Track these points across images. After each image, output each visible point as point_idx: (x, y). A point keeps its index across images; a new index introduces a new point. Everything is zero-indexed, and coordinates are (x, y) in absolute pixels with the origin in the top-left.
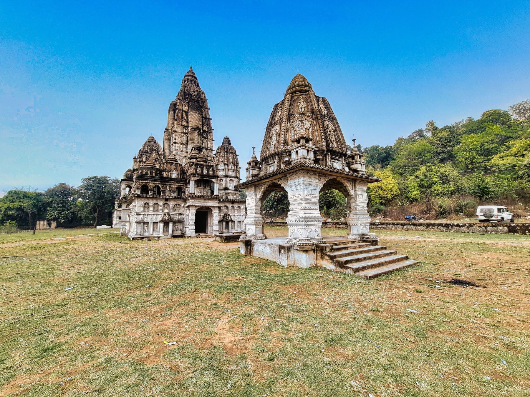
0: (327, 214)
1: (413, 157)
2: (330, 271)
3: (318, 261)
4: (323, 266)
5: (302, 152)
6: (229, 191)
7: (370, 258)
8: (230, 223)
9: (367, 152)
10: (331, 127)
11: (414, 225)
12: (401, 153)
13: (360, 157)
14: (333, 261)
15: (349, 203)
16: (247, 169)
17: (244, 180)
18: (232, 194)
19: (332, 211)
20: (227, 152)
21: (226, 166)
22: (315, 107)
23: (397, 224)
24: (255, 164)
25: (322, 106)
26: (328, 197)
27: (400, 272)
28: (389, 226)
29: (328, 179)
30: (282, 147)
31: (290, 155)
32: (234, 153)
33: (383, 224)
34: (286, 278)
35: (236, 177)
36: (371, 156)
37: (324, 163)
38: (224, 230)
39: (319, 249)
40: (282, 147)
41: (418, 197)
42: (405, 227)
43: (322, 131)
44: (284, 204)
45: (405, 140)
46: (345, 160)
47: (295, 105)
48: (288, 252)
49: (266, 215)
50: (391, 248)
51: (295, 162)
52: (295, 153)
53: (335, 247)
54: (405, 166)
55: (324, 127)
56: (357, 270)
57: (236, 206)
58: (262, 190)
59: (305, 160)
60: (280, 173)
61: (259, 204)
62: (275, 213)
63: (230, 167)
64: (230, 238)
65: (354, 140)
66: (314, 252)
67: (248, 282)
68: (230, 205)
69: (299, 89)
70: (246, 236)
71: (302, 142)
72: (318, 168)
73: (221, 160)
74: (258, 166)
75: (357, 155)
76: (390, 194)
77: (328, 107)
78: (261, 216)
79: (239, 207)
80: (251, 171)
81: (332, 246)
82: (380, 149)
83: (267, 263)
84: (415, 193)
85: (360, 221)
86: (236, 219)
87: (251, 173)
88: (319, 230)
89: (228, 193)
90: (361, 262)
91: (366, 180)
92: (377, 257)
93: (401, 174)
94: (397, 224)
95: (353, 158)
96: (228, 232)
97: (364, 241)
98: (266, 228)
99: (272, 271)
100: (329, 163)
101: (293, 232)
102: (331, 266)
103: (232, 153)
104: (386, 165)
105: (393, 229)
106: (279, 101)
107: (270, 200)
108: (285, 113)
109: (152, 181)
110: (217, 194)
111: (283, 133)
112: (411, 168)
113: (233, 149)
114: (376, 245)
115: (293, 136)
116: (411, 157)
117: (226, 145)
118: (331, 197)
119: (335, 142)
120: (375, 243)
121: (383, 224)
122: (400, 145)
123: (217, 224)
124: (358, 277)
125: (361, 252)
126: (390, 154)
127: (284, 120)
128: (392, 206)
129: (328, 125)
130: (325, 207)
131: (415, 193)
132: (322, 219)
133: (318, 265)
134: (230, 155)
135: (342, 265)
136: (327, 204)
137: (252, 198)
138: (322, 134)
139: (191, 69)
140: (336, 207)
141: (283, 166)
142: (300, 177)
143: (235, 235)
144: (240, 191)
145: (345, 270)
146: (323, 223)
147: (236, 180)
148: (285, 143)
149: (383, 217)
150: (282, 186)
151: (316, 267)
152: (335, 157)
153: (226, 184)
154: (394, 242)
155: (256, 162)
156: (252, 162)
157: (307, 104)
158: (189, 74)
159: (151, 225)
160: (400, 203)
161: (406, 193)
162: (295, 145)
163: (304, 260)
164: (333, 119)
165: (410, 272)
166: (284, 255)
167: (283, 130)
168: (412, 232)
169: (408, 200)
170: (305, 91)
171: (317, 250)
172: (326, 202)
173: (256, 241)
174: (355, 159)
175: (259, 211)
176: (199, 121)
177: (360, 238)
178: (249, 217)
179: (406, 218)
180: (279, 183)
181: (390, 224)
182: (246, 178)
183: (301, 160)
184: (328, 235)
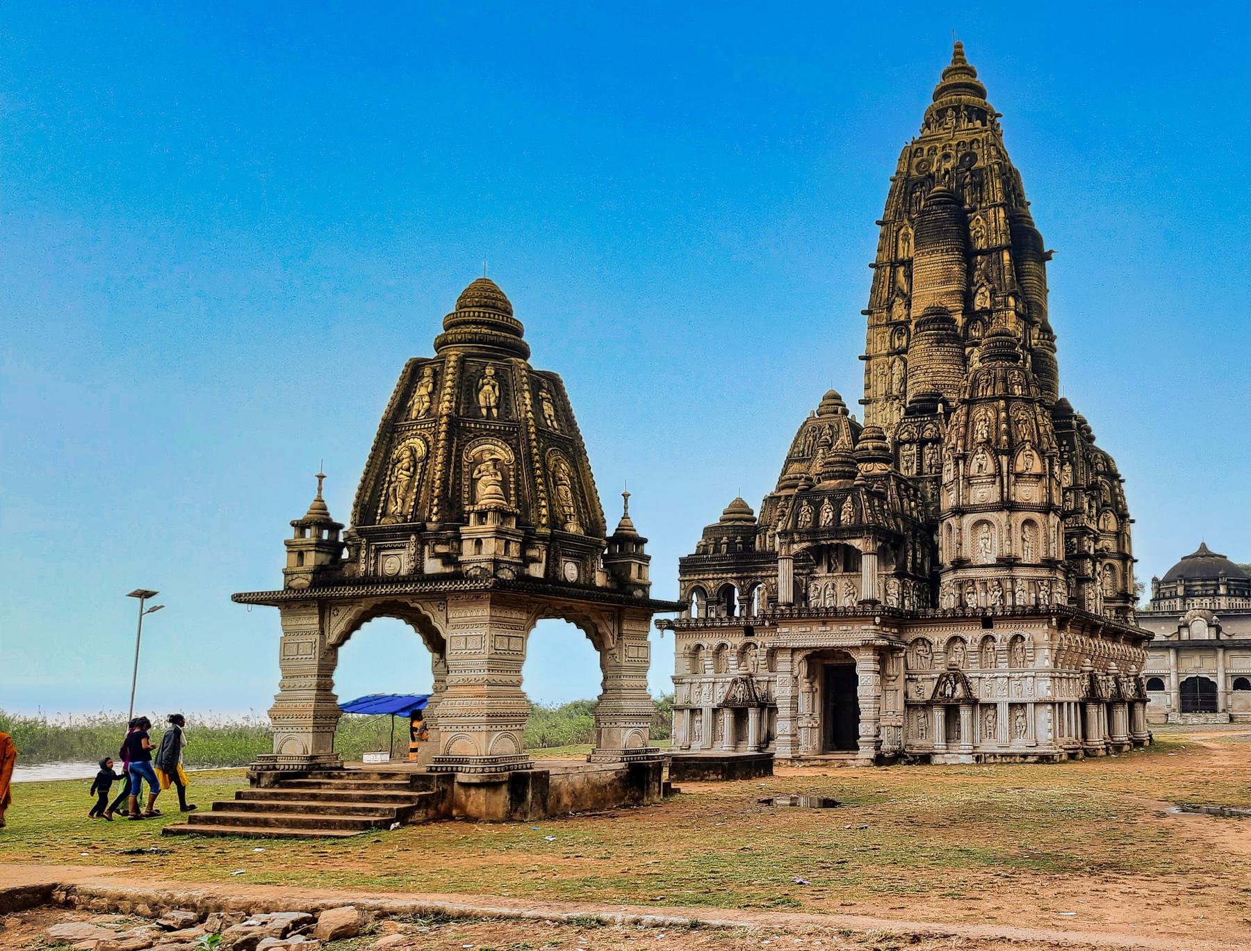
6: (971, 573)
8: (965, 713)
21: (1004, 460)
57: (1003, 633)
63: (974, 469)
64: (687, 767)
68: (973, 634)
69: (487, 334)
109: (716, 571)
139: (959, 52)
158: (951, 81)
159: (707, 715)
176: (947, 281)
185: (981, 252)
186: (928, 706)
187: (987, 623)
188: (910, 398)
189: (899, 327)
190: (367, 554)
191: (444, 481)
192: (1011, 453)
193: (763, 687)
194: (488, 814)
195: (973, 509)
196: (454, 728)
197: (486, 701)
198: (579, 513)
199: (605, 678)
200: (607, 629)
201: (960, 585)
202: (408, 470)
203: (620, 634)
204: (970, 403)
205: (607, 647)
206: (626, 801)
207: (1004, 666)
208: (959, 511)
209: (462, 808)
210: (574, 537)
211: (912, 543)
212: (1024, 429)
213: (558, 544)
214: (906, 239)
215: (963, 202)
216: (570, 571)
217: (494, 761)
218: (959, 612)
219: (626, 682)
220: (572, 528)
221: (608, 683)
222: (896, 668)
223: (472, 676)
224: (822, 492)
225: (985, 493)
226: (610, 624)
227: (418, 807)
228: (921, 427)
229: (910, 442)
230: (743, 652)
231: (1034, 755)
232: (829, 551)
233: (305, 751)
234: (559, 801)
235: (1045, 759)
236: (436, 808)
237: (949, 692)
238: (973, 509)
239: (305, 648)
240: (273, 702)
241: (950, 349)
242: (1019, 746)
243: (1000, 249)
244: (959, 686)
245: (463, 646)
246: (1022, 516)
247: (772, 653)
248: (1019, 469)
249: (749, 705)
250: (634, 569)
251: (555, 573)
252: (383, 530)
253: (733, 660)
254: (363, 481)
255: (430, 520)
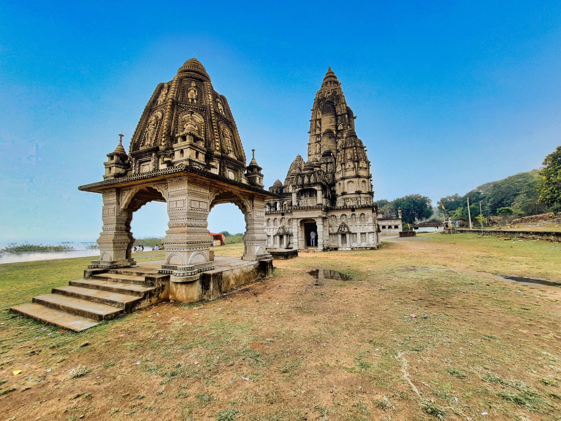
6: (347, 196)
8: (348, 236)
21: (356, 164)
57: (358, 213)
63: (347, 167)
68: (349, 213)
69: (195, 75)
139: (330, 69)
141: (162, 167)
152: (144, 159)
159: (272, 237)
176: (331, 122)
180: (155, 188)
185: (339, 115)
186: (336, 234)
187: (353, 210)
188: (322, 153)
189: (318, 136)
190: (135, 165)
191: (169, 127)
192: (358, 162)
193: (287, 229)
194: (187, 299)
195: (347, 178)
196: (171, 250)
197: (186, 235)
198: (234, 151)
199: (247, 225)
200: (247, 203)
201: (344, 199)
202: (154, 125)
203: (253, 206)
204: (345, 149)
205: (248, 211)
206: (259, 277)
207: (359, 222)
208: (343, 179)
209: (174, 294)
210: (231, 159)
211: (329, 188)
212: (361, 155)
213: (224, 160)
214: (319, 114)
215: (333, 103)
216: (231, 175)
217: (192, 268)
218: (345, 207)
219: (256, 226)
220: (231, 155)
221: (249, 227)
222: (326, 224)
223: (180, 222)
224: (304, 174)
225: (351, 173)
226: (249, 201)
227: (144, 298)
228: (327, 159)
229: (324, 163)
230: (281, 220)
232: (306, 191)
233: (111, 259)
234: (228, 283)
235: (372, 249)
236: (158, 296)
237: (343, 230)
238: (347, 178)
239: (111, 211)
240: (99, 236)
241: (333, 139)
242: (364, 245)
243: (345, 114)
245: (175, 206)
246: (362, 179)
247: (289, 220)
248: (360, 166)
249: (283, 235)
250: (258, 179)
251: (224, 175)
252: (141, 153)
253: (278, 222)
254: (135, 133)
255: (161, 145)
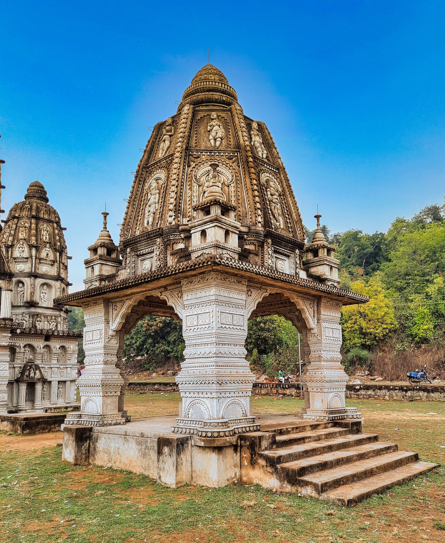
0: (257, 365)
1: (422, 258)
2: (269, 492)
3: (244, 472)
4: (255, 481)
5: (215, 234)
6: (39, 311)
7: (348, 460)
8: (39, 387)
9: (338, 242)
10: (275, 185)
11: (425, 390)
12: (401, 249)
13: (329, 251)
14: (276, 469)
15: (306, 345)
16: (87, 263)
17: (77, 286)
18: (46, 316)
19: (270, 359)
20: (37, 218)
21: (34, 251)
22: (243, 140)
23: (394, 389)
24: (108, 252)
25: (257, 140)
26: (262, 329)
27: (405, 488)
28: (379, 392)
29: (267, 294)
30: (170, 219)
31: (188, 238)
32: (55, 221)
33: (367, 388)
34: (173, 514)
35: (58, 278)
36: (346, 251)
37: (258, 259)
38: (23, 403)
39: (246, 445)
40: (170, 219)
41: (430, 335)
42: (409, 394)
43: (256, 193)
44: (169, 343)
45: (408, 226)
46: (301, 257)
47: (202, 130)
48: (178, 453)
49: (127, 367)
50: (386, 438)
51: (199, 253)
52: (198, 235)
53: (278, 438)
54: (407, 274)
55: (259, 184)
56: (324, 488)
57: (55, 345)
58: (123, 310)
59: (220, 251)
60: (166, 276)
61: (115, 343)
62: (149, 361)
63: (43, 254)
64: (38, 424)
65: (318, 217)
66: (236, 450)
67: (81, 531)
68: (39, 344)
70: (80, 416)
71: (216, 211)
72: (258, 274)
73: (21, 236)
74: (114, 256)
75: (324, 247)
76: (380, 329)
77: (268, 144)
78: (118, 371)
79: (63, 347)
80: (97, 268)
81: (274, 437)
82: (363, 237)
83: (129, 481)
84: (426, 327)
85: (328, 383)
86: (53, 376)
87: (97, 272)
88: (245, 402)
89: (38, 315)
90: (332, 471)
91: (340, 299)
92: (362, 457)
93: (400, 289)
94: (394, 389)
95: (316, 254)
96: (33, 408)
97: (335, 424)
98: (127, 396)
99: (141, 499)
100: (269, 261)
101: (192, 405)
102: (272, 482)
103: (49, 221)
104: (374, 270)
105: (387, 397)
106: (167, 117)
107: (137, 333)
108: (180, 145)
110: (8, 316)
111: (174, 188)
112: (418, 278)
113: (51, 211)
114: (358, 431)
115: (194, 196)
116: (417, 257)
117: (35, 202)
118: (268, 330)
119: (281, 219)
120: (356, 427)
121: (367, 388)
122: (398, 232)
123: (5, 388)
124: (326, 502)
125: (330, 448)
126: (380, 250)
127: (176, 160)
128: (383, 351)
129: (267, 181)
130: (255, 351)
131: (425, 327)
132: (253, 377)
133: (245, 479)
134: (44, 226)
135: (294, 478)
136: (260, 345)
137: (99, 330)
138: (257, 199)
140: (276, 351)
141: (171, 261)
142: (209, 286)
143: (49, 414)
144: (67, 312)
145: (300, 489)
146: (255, 385)
147: (58, 284)
148: (178, 210)
149: (367, 372)
150: (169, 304)
151: (240, 484)
152: (282, 250)
153: (32, 294)
154: (389, 425)
155: (110, 249)
156: (101, 246)
157: (227, 130)
160: (398, 346)
161: (409, 327)
162: (200, 217)
163: (213, 470)
164: (279, 170)
165: (422, 487)
166: (169, 461)
167: (174, 182)
168: (420, 404)
169: (413, 340)
170: (224, 102)
171: (241, 446)
172: (257, 339)
173: (104, 429)
174: (320, 255)
175: (115, 359)
177: (326, 417)
178: (89, 372)
179: (410, 377)
180: (163, 297)
181: (380, 388)
182: (86, 282)
183: (213, 251)
184: (262, 411)
187: (48, 337)
231: (71, 407)
238: (42, 276)
244: (37, 372)
